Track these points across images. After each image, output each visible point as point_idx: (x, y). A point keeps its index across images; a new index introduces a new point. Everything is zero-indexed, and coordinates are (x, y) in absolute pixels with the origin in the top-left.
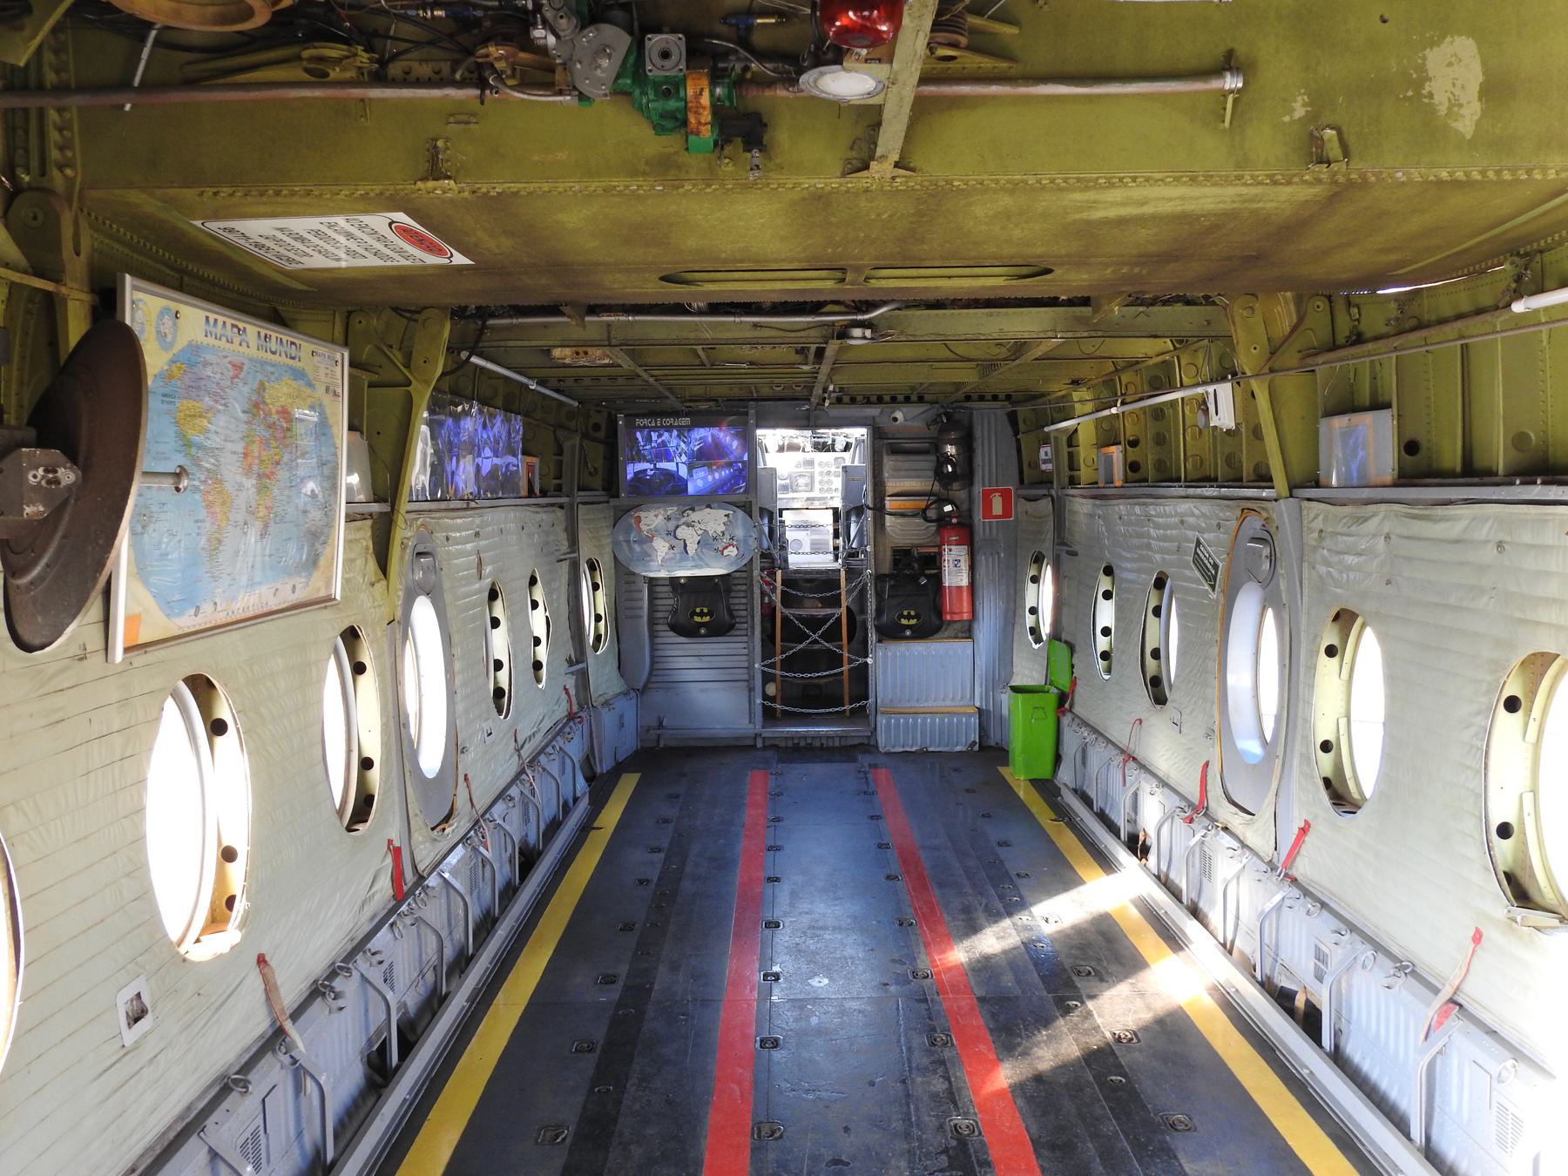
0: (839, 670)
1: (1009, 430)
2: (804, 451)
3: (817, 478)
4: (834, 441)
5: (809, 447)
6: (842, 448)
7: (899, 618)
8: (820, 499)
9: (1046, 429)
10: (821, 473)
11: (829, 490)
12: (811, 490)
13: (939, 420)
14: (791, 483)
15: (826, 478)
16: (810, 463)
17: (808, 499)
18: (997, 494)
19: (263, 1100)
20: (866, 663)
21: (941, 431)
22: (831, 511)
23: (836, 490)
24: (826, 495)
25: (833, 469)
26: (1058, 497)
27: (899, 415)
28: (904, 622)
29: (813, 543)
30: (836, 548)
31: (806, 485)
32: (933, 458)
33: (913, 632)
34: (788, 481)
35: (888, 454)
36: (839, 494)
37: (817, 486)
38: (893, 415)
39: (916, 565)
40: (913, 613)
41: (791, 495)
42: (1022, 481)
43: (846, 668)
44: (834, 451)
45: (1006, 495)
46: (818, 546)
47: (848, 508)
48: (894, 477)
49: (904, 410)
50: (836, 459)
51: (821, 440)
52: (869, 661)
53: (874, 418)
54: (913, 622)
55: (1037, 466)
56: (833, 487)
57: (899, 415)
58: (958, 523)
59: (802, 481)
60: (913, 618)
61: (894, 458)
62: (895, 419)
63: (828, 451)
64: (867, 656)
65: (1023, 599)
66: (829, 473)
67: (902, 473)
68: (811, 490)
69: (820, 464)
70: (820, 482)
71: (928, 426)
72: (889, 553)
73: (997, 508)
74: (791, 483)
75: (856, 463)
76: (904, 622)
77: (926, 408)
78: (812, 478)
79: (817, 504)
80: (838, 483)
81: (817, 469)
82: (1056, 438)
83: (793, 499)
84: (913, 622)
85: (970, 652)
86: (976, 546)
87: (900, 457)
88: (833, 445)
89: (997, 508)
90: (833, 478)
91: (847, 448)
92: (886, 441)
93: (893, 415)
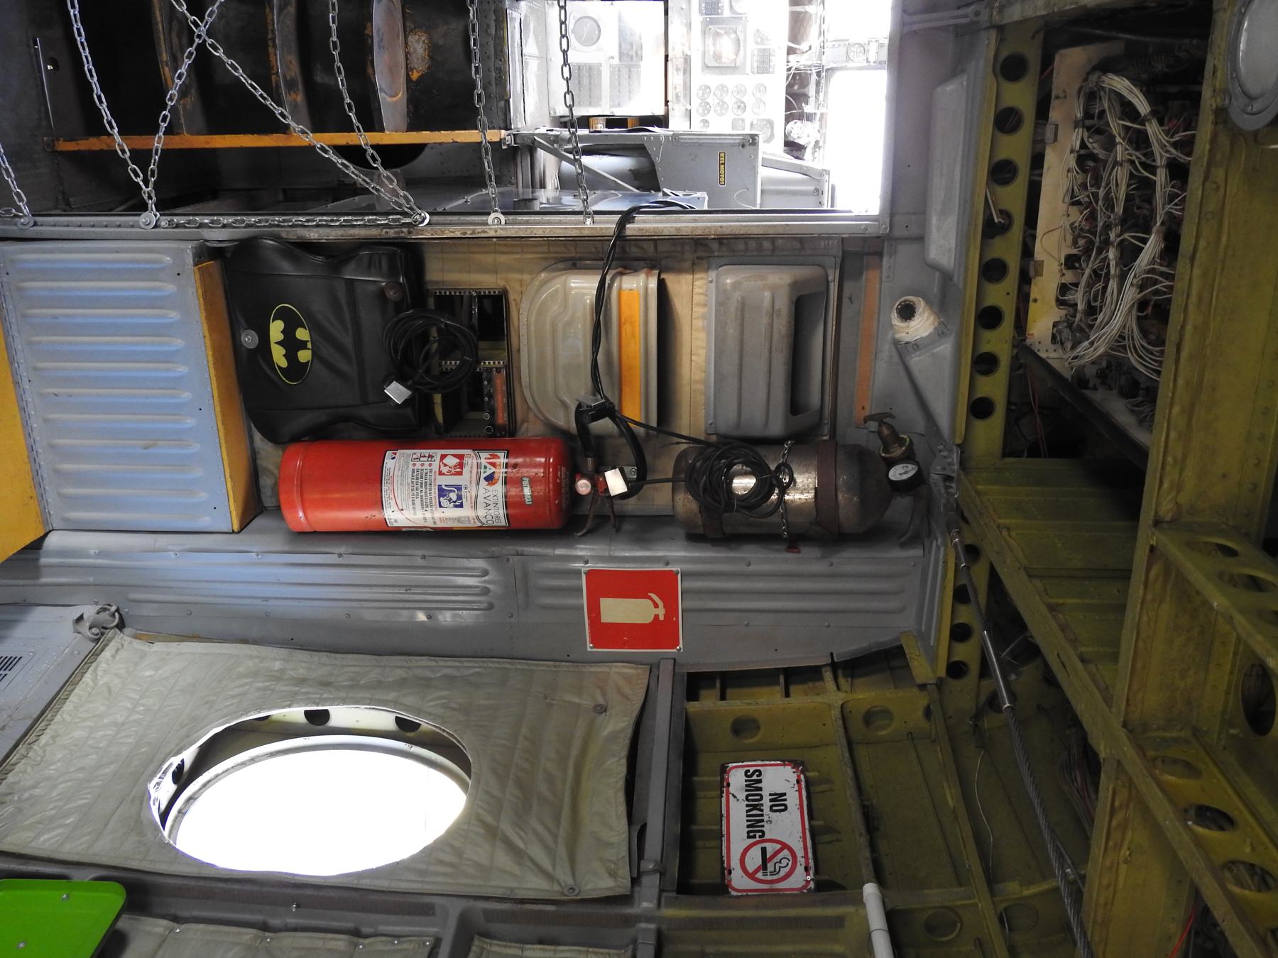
0: (362, 130)
1: (846, 647)
2: (790, 51)
3: (730, 80)
4: (809, 117)
5: (798, 61)
6: (794, 137)
7: (283, 315)
8: (687, 86)
9: (870, 890)
10: (741, 90)
11: (706, 107)
12: (706, 67)
13: (898, 451)
14: (722, 21)
15: (730, 100)
16: (764, 66)
17: (687, 60)
18: (661, 612)
19: (600, 31)
20: (143, 207)
21: (860, 455)
22: (660, 111)
23: (705, 122)
24: (696, 101)
25: (749, 117)
26: (629, 921)
27: (921, 326)
28: (276, 329)
29: (591, 71)
30: (585, 122)
31: (717, 57)
32: (776, 428)
33: (252, 353)
34: (727, 13)
35: (795, 285)
36: (697, 128)
37: (714, 80)
38: (921, 305)
39: (452, 364)
40: (304, 356)
41: (697, 19)
42: (694, 684)
43: (119, 143)
44: (788, 119)
45: (659, 633)
46: (585, 81)
47: (652, 150)
48: (721, 304)
49: (945, 348)
50: (770, 123)
51: (811, 90)
52: (150, 216)
53: (921, 239)
54: (279, 356)
55: (741, 755)
56: (711, 117)
57: (921, 326)
58: (576, 497)
59: (726, 46)
60: (291, 356)
61: (783, 304)
62: (907, 312)
63: (789, 106)
64: (162, 206)
65: (344, 701)
66: (741, 106)
67: (732, 331)
68: (706, 67)
69: (762, 88)
70: (722, 88)
71: (880, 418)
72: (487, 281)
73: (616, 610)
74: (722, 21)
75: (763, 172)
76: (276, 329)
77: (943, 421)
78: (732, 69)
79: (676, 79)
80: (720, 125)
81: (750, 80)
82: (839, 922)
83: (689, 25)
84: (279, 356)
85: (205, 522)
86: (509, 548)
87: (782, 325)
88: (801, 117)
89: (616, 610)
90: (730, 116)
91: (793, 147)
92: (833, 275)
93: (921, 305)
